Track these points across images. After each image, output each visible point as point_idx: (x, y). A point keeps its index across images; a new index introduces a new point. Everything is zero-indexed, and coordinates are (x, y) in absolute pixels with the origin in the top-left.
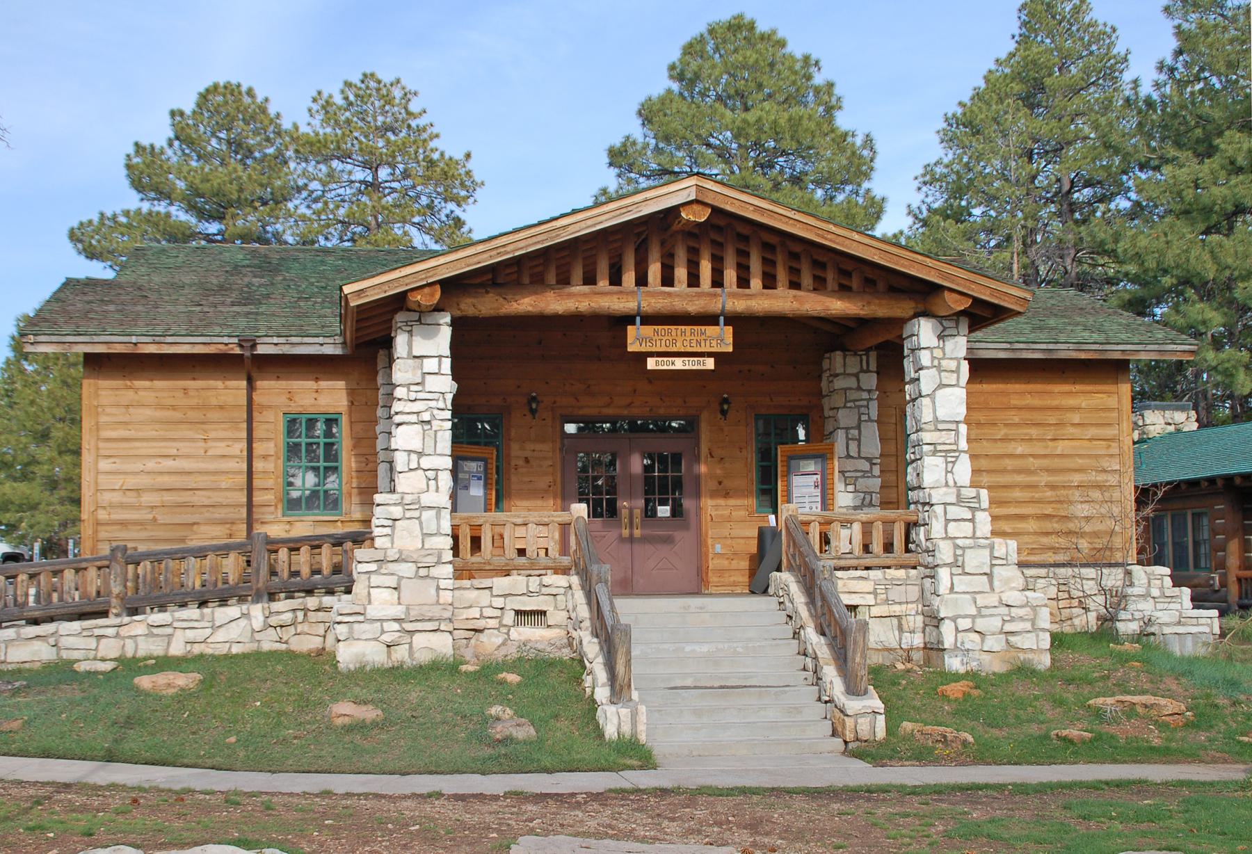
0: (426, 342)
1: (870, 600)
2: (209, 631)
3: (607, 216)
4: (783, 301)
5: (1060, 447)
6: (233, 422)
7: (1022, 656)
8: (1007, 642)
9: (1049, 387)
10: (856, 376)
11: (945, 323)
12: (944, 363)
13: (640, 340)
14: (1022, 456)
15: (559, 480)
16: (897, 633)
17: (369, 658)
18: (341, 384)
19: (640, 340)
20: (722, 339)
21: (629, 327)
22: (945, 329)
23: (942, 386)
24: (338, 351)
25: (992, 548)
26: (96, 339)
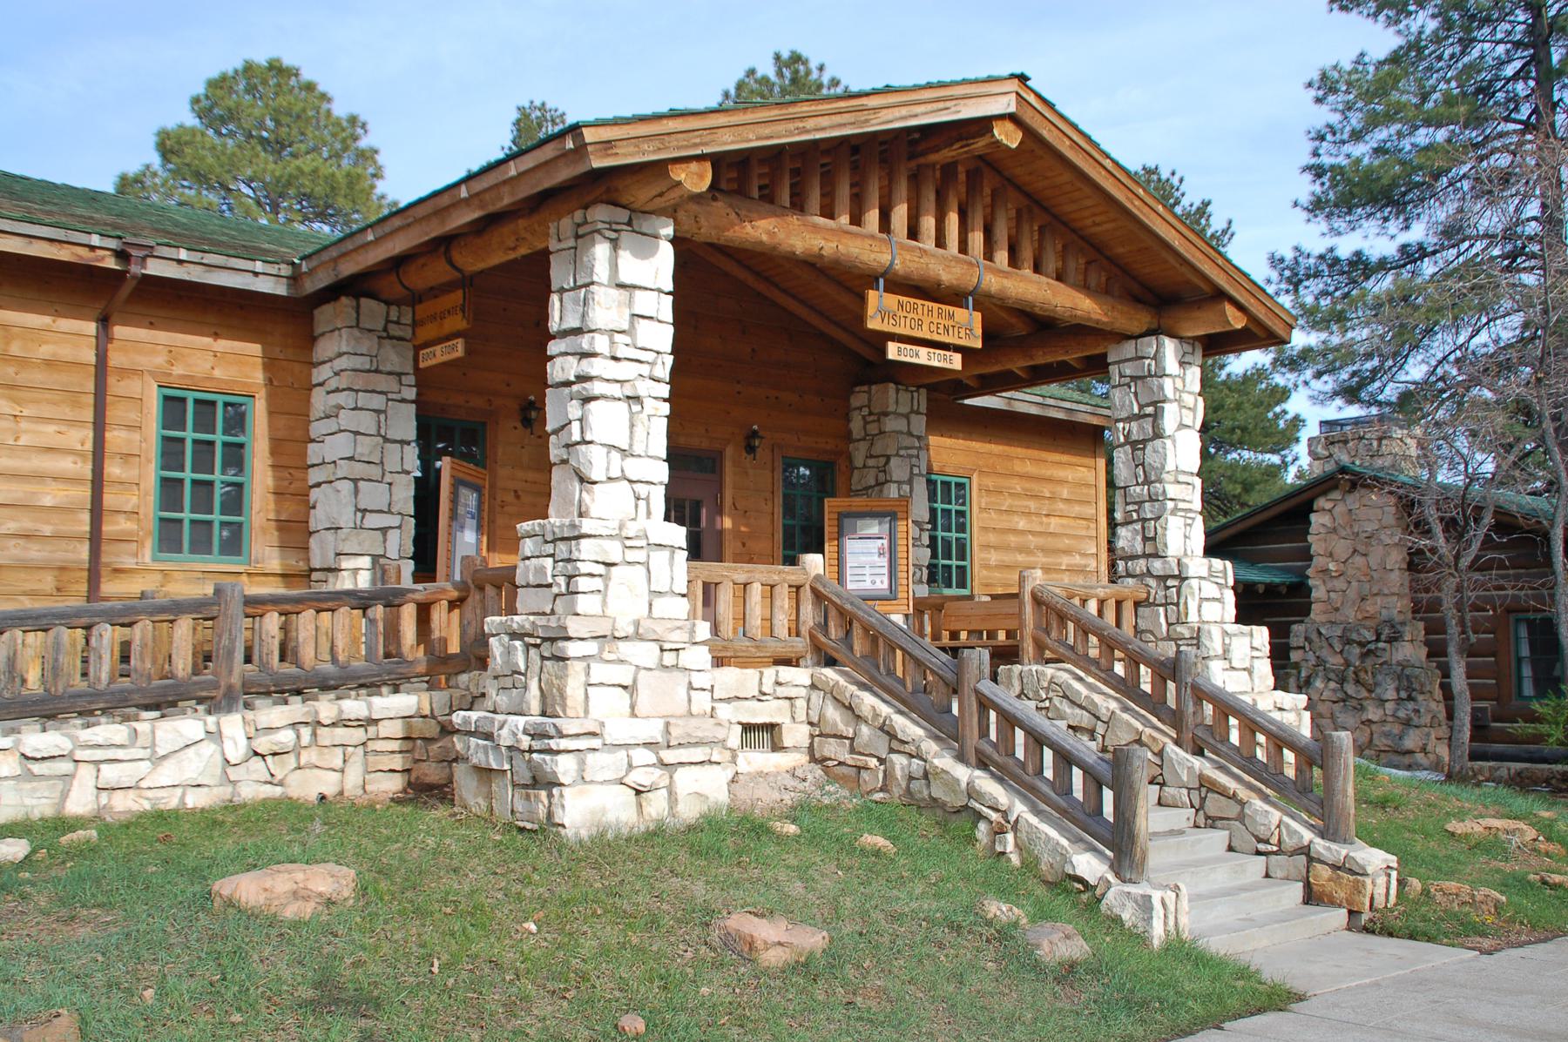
0: (638, 262)
5: (1054, 524)
6: (73, 396)
9: (1044, 455)
10: (907, 417)
13: (884, 314)
14: (1023, 532)
17: (611, 817)
18: (255, 349)
19: (884, 314)
24: (281, 289)
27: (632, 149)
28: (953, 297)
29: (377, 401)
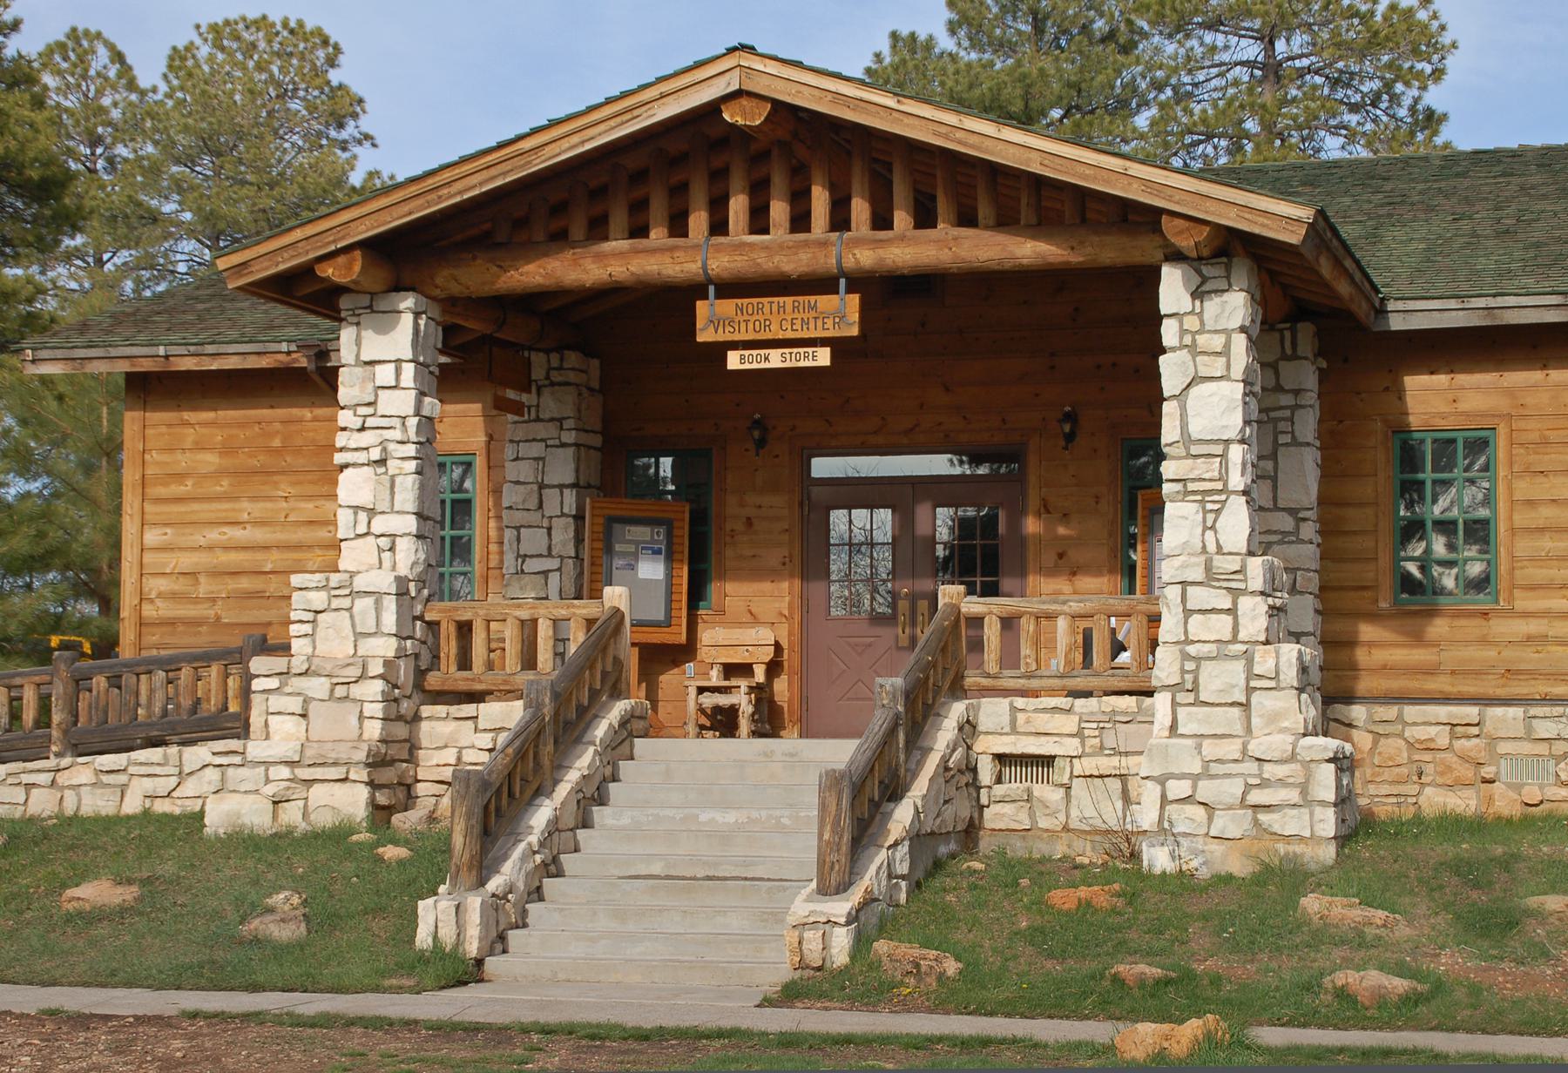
1: (1072, 746)
2: (173, 781)
3: (602, 127)
4: (909, 248)
7: (1281, 848)
8: (1256, 822)
11: (1206, 270)
12: (1201, 339)
13: (715, 322)
15: (797, 552)
16: (1119, 804)
17: (247, 821)
18: (478, 406)
20: (842, 314)
21: (699, 304)
22: (1204, 280)
23: (1196, 380)
25: (1250, 663)
26: (114, 352)
27: (266, 264)
28: (821, 284)
29: (536, 449)
